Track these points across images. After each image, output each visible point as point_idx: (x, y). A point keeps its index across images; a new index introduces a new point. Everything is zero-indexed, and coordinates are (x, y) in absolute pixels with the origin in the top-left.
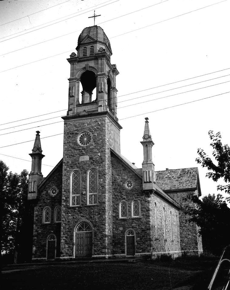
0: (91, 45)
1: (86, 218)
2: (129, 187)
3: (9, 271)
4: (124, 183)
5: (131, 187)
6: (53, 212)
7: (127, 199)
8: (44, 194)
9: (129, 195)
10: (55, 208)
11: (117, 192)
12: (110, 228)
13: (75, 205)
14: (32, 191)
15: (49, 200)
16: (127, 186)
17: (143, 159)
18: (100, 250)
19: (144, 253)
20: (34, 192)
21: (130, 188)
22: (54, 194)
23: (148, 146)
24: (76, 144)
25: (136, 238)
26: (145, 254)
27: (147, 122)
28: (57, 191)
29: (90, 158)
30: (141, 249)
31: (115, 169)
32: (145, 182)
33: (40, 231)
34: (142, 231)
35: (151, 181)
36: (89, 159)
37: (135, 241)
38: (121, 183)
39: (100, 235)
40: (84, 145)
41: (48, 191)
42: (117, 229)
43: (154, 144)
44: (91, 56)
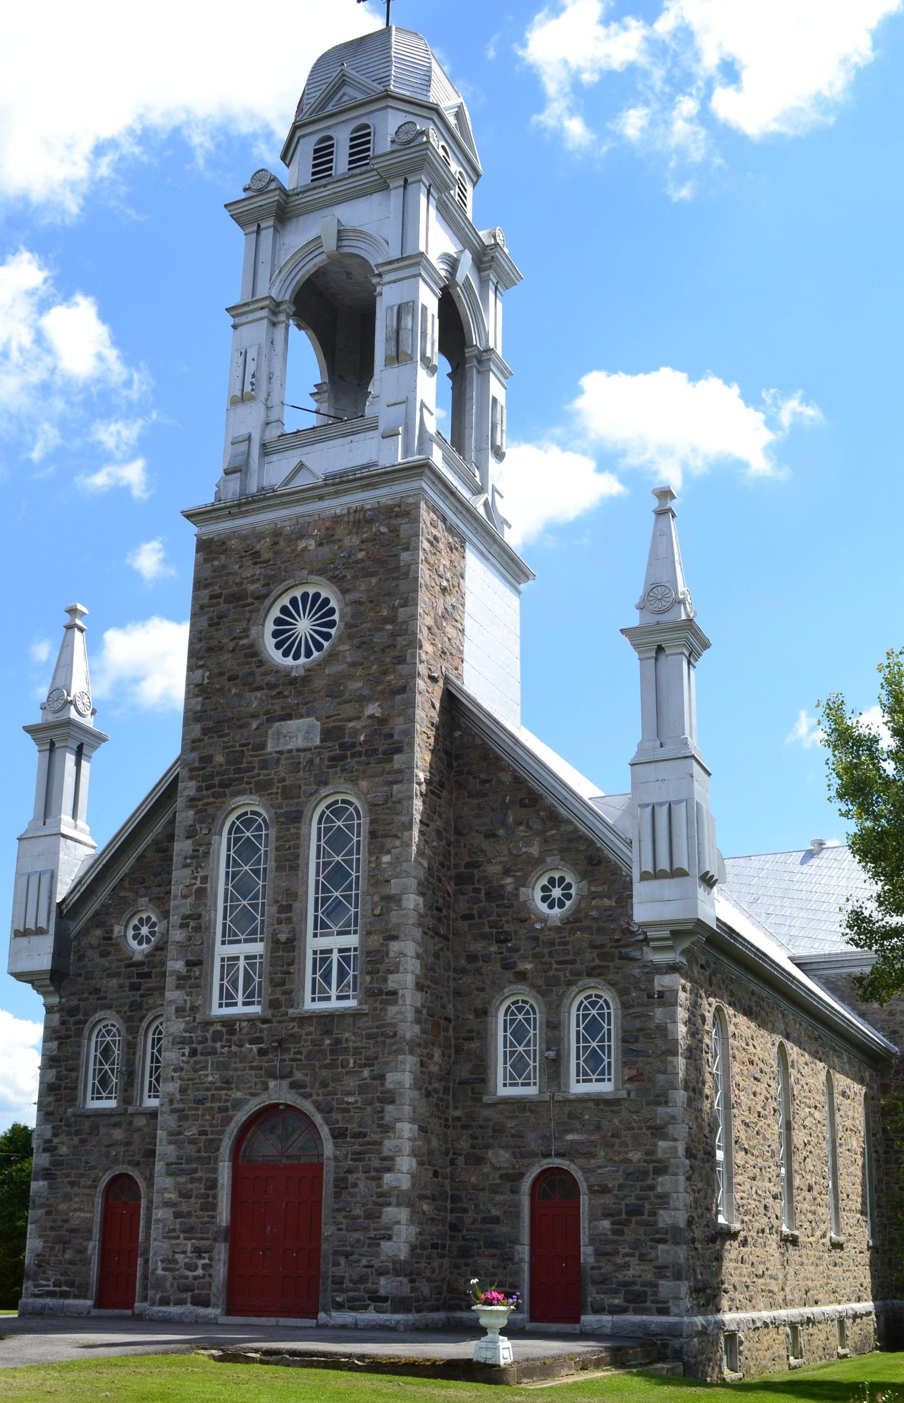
0: (357, 123)
1: (294, 1086)
2: (551, 906)
3: (549, 1385)
4: (522, 882)
5: (561, 905)
6: (131, 1047)
7: (541, 982)
8: (91, 947)
9: (551, 955)
10: (144, 1025)
11: (484, 936)
12: (431, 1152)
13: (328, 998)
14: (664, 864)
15: (117, 975)
16: (544, 899)
17: (637, 735)
18: (363, 1279)
19: (637, 1318)
20: (40, 931)
21: (556, 911)
22: (144, 946)
23: (668, 652)
24: (253, 653)
25: (590, 1221)
26: (644, 1326)
27: (663, 513)
28: (573, 891)
29: (327, 735)
30: (615, 1292)
31: (475, 802)
32: (645, 876)
33: (64, 1150)
34: (628, 1175)
35: (682, 862)
36: (317, 742)
37: (584, 1238)
38: (509, 880)
39: (363, 1186)
40: (296, 657)
41: (112, 926)
42: (480, 1160)
43: (706, 645)
44: (316, 184)
